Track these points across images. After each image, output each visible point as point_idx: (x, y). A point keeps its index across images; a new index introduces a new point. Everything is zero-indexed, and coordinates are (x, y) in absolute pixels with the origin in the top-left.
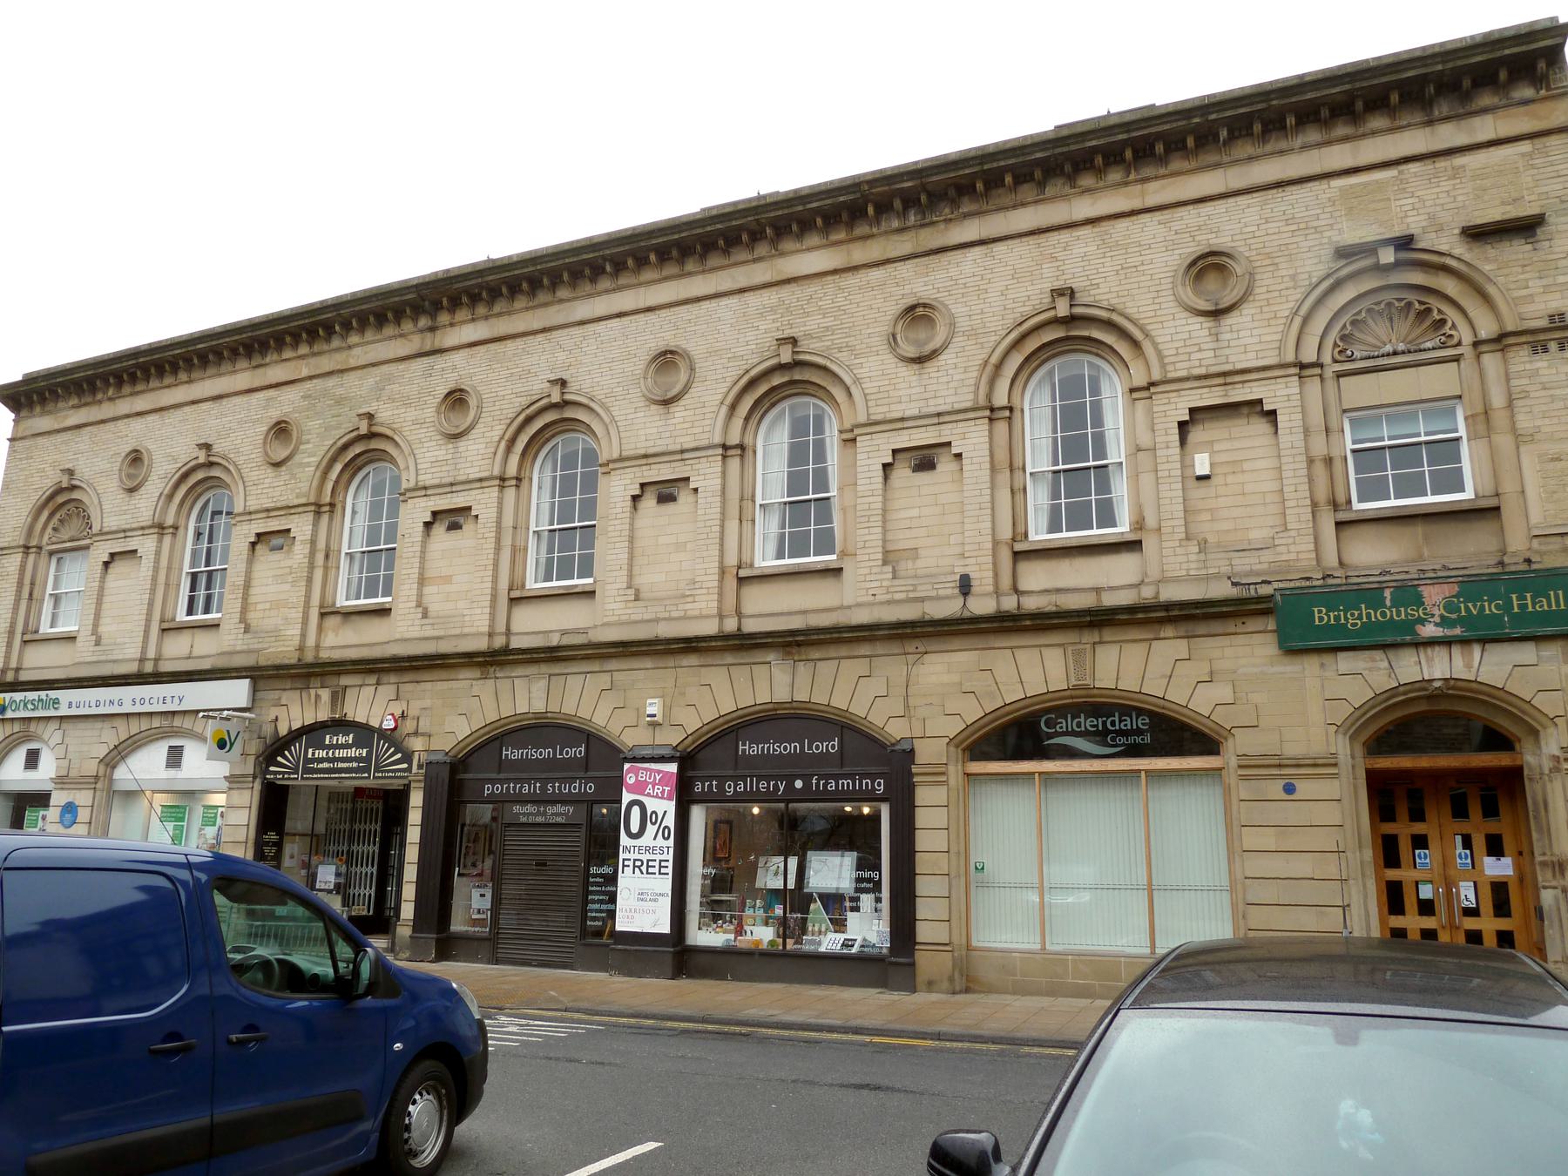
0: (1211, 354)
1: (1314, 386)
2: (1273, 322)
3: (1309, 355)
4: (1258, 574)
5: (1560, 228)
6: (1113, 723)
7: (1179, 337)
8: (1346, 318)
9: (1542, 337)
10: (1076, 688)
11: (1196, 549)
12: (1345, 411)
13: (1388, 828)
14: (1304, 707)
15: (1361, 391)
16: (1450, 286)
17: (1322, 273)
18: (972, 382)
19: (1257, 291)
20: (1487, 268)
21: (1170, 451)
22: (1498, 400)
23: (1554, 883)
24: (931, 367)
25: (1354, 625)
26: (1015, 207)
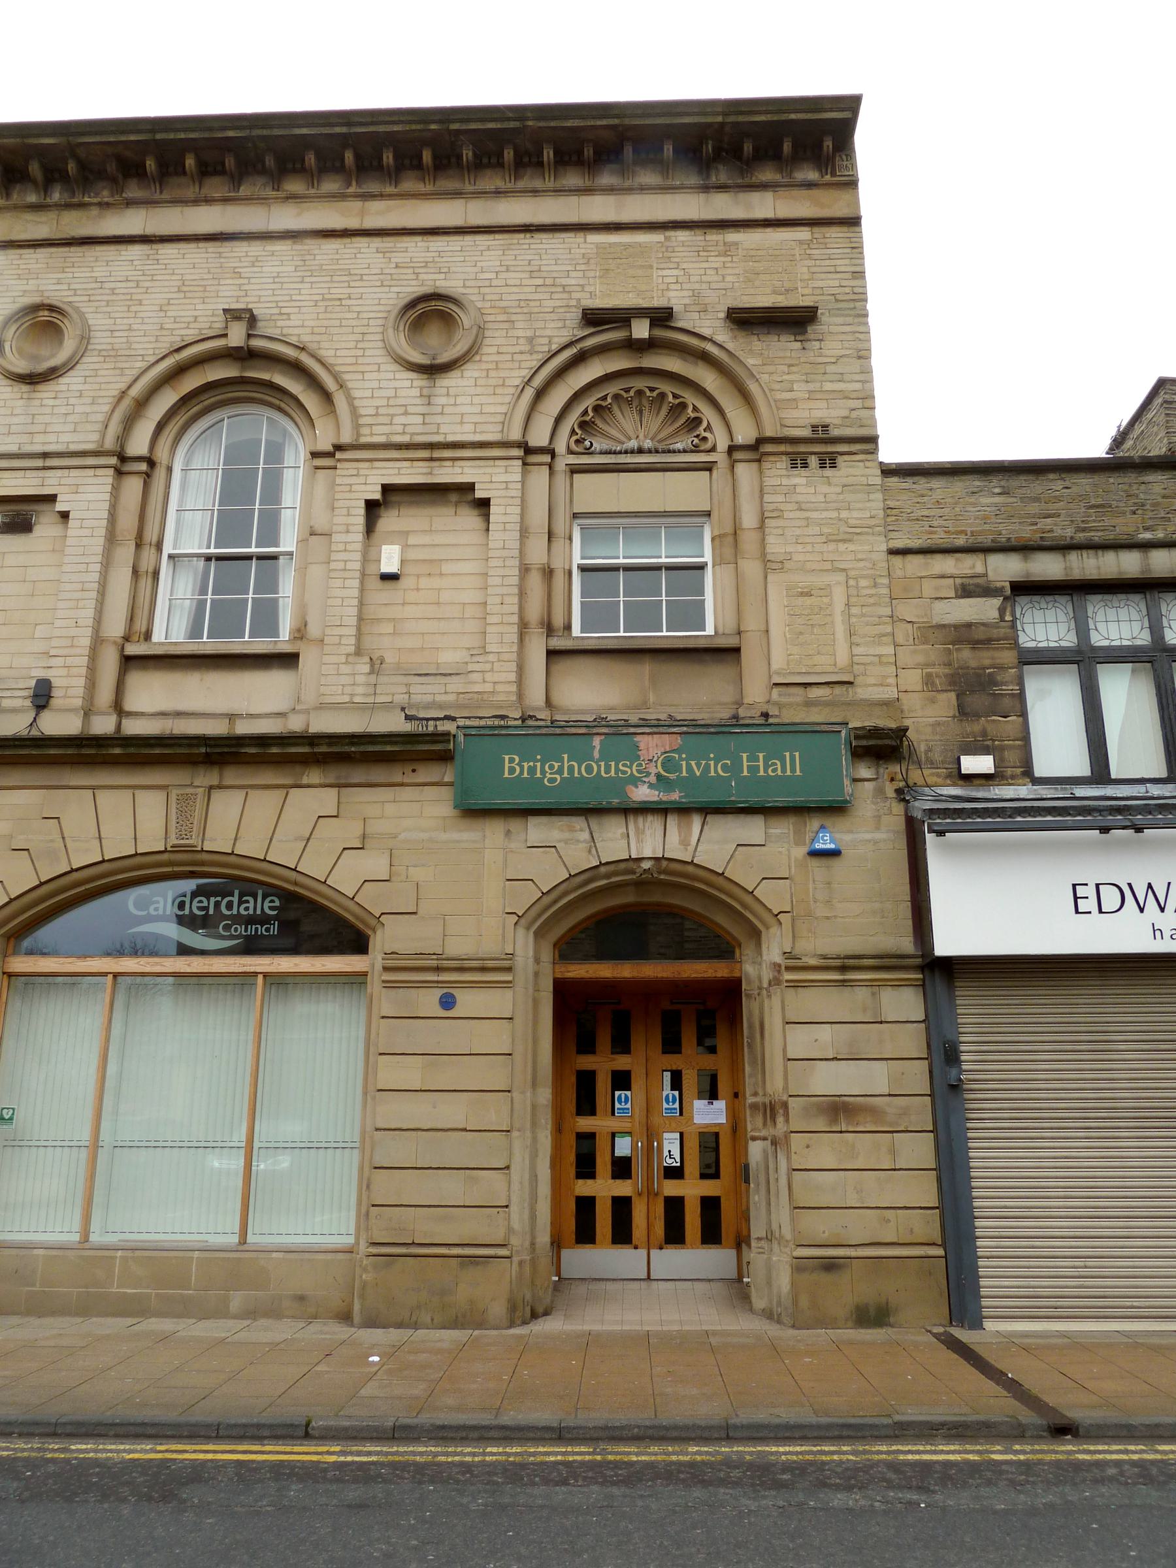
0: (419, 419)
1: (540, 477)
2: (499, 391)
3: (539, 437)
4: (441, 707)
5: (833, 329)
6: (229, 906)
7: (382, 395)
8: (589, 402)
9: (802, 448)
10: (177, 849)
11: (366, 668)
12: (575, 516)
13: (586, 1062)
14: (461, 885)
15: (597, 492)
16: (709, 379)
17: (564, 341)
18: (100, 417)
19: (485, 350)
20: (750, 362)
21: (351, 537)
22: (749, 520)
23: (763, 1133)
24: (46, 391)
25: (551, 780)
26: (196, 202)
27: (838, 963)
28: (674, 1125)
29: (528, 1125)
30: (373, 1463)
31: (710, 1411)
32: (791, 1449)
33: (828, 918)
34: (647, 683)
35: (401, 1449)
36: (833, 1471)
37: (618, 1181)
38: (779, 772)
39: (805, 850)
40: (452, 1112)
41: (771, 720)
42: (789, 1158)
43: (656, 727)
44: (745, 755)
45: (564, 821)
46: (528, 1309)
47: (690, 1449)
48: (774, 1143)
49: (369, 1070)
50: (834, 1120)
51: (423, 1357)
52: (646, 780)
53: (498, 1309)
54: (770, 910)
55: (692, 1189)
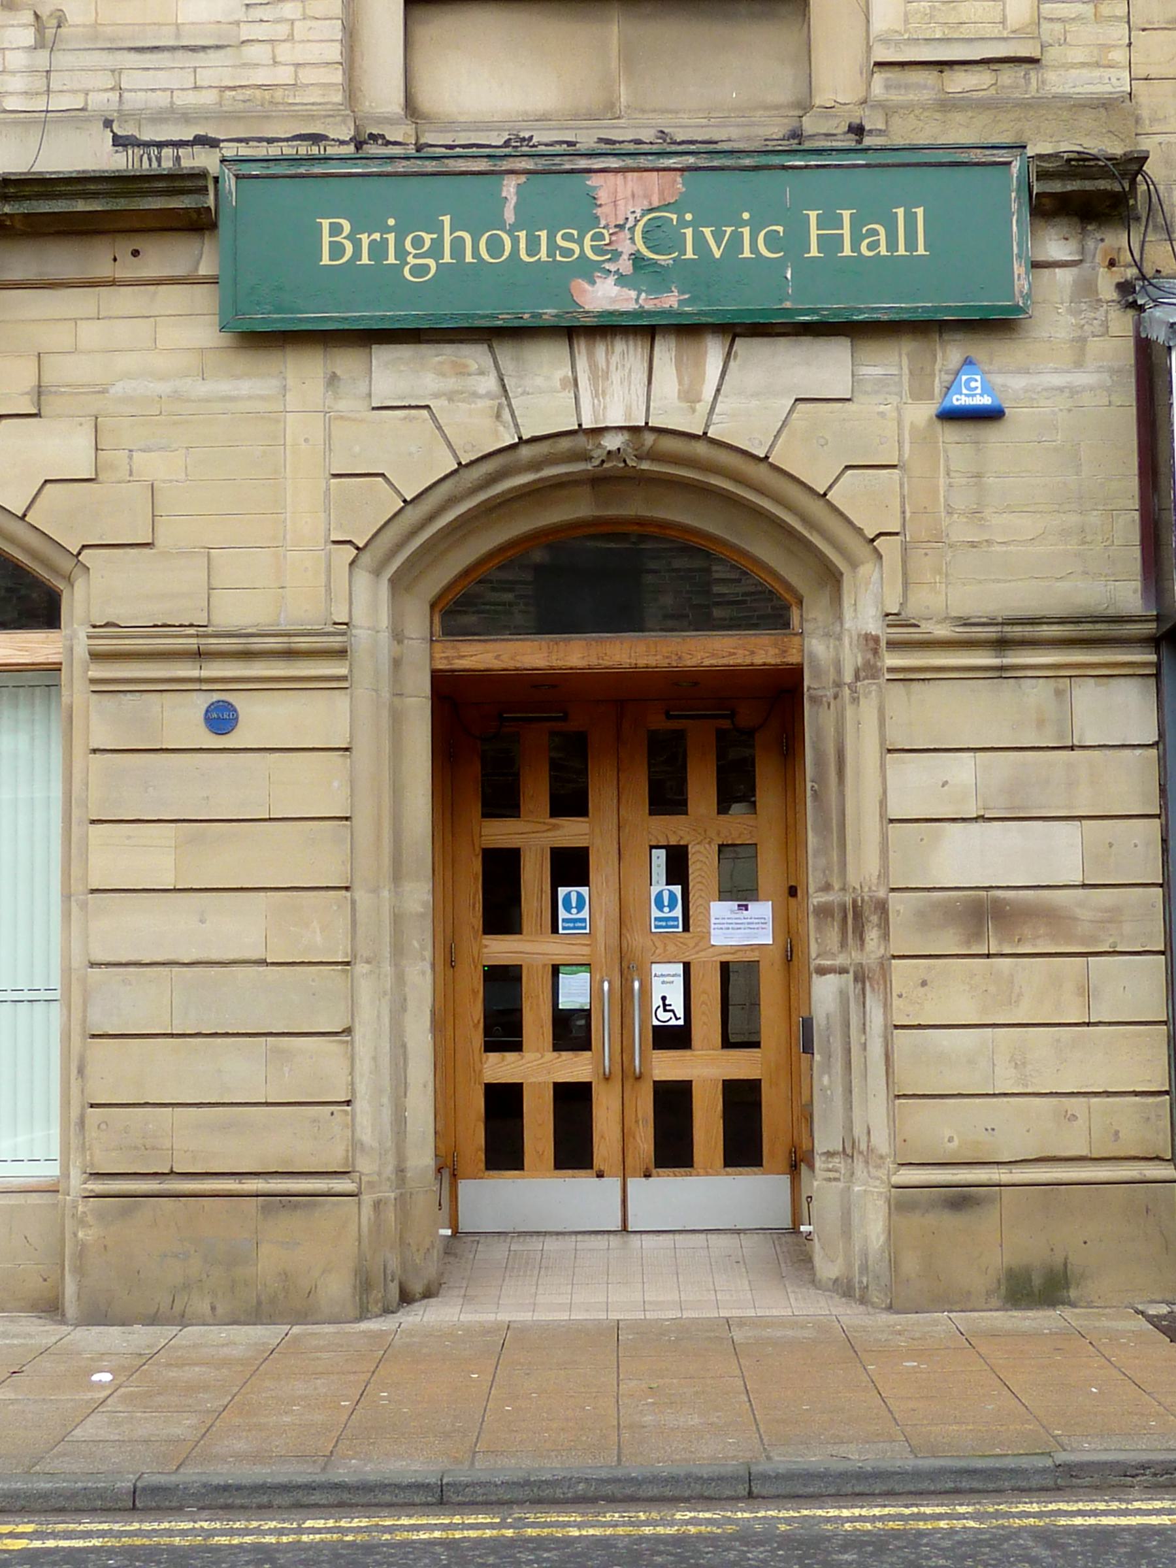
4: (186, 117)
11: (28, 37)
13: (500, 833)
23: (840, 960)
25: (419, 270)
27: (991, 633)
28: (671, 948)
29: (386, 952)
30: (94, 1550)
31: (719, 1450)
32: (864, 1512)
33: (973, 545)
34: (614, 64)
35: (146, 1526)
36: (934, 1546)
37: (565, 1055)
38: (883, 250)
39: (929, 409)
40: (239, 929)
41: (868, 141)
42: (887, 1006)
43: (633, 157)
44: (813, 215)
45: (446, 353)
46: (394, 1288)
47: (678, 1516)
48: (861, 977)
49: (72, 853)
50: (977, 935)
51: (193, 1373)
52: (612, 267)
53: (337, 1287)
54: (859, 531)
55: (706, 1068)
